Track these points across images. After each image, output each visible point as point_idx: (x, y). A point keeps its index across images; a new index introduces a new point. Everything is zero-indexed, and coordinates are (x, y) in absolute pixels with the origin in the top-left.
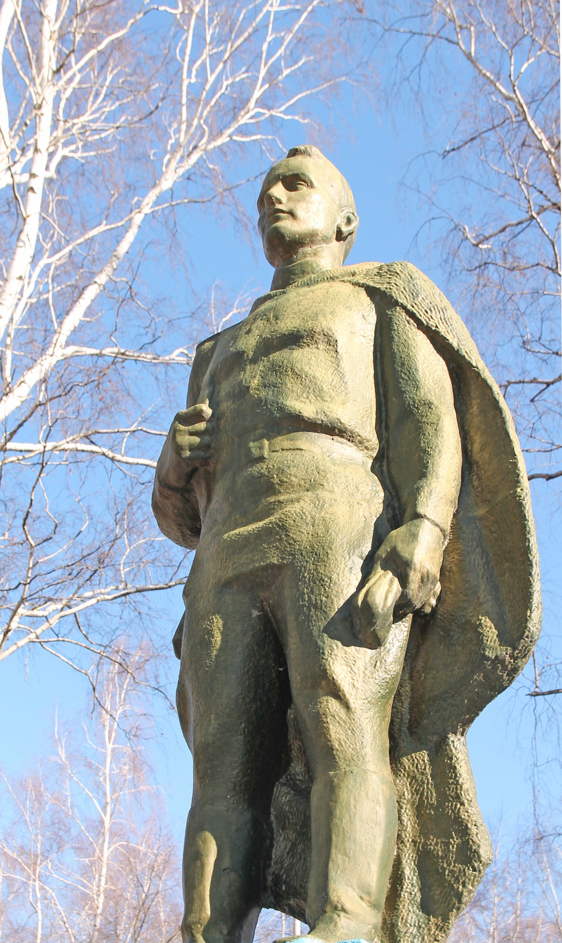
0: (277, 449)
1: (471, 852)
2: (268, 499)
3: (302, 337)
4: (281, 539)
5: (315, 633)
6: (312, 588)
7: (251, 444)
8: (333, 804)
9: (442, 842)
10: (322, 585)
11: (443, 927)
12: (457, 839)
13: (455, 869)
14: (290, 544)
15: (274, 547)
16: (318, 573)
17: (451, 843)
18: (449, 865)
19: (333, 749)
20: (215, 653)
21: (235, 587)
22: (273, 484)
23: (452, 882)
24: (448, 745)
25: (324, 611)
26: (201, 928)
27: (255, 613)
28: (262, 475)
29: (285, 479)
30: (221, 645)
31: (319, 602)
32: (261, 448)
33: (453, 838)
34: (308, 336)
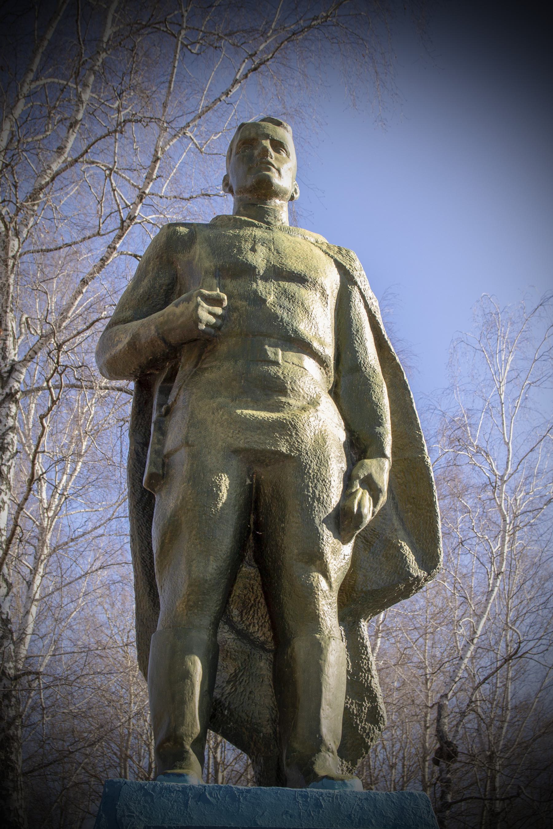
0: (289, 361)
1: (379, 716)
2: (280, 398)
3: (308, 281)
4: (291, 436)
5: (317, 521)
6: (316, 484)
7: (266, 347)
8: (323, 662)
9: (356, 703)
10: (324, 485)
11: (351, 770)
12: (368, 703)
13: (366, 727)
14: (298, 442)
15: (284, 439)
16: (321, 474)
17: (364, 706)
18: (361, 722)
19: (319, 617)
20: (220, 505)
21: (241, 456)
22: (286, 388)
23: (364, 737)
24: (360, 627)
25: (325, 506)
26: (191, 740)
27: (248, 482)
28: (278, 378)
29: (295, 388)
30: (226, 500)
31: (322, 498)
32: (276, 354)
33: (365, 702)
34: (311, 282)
